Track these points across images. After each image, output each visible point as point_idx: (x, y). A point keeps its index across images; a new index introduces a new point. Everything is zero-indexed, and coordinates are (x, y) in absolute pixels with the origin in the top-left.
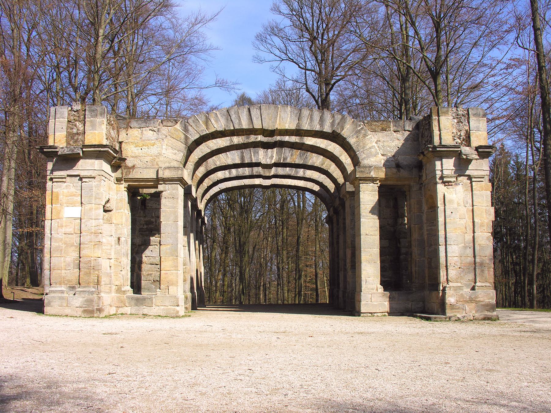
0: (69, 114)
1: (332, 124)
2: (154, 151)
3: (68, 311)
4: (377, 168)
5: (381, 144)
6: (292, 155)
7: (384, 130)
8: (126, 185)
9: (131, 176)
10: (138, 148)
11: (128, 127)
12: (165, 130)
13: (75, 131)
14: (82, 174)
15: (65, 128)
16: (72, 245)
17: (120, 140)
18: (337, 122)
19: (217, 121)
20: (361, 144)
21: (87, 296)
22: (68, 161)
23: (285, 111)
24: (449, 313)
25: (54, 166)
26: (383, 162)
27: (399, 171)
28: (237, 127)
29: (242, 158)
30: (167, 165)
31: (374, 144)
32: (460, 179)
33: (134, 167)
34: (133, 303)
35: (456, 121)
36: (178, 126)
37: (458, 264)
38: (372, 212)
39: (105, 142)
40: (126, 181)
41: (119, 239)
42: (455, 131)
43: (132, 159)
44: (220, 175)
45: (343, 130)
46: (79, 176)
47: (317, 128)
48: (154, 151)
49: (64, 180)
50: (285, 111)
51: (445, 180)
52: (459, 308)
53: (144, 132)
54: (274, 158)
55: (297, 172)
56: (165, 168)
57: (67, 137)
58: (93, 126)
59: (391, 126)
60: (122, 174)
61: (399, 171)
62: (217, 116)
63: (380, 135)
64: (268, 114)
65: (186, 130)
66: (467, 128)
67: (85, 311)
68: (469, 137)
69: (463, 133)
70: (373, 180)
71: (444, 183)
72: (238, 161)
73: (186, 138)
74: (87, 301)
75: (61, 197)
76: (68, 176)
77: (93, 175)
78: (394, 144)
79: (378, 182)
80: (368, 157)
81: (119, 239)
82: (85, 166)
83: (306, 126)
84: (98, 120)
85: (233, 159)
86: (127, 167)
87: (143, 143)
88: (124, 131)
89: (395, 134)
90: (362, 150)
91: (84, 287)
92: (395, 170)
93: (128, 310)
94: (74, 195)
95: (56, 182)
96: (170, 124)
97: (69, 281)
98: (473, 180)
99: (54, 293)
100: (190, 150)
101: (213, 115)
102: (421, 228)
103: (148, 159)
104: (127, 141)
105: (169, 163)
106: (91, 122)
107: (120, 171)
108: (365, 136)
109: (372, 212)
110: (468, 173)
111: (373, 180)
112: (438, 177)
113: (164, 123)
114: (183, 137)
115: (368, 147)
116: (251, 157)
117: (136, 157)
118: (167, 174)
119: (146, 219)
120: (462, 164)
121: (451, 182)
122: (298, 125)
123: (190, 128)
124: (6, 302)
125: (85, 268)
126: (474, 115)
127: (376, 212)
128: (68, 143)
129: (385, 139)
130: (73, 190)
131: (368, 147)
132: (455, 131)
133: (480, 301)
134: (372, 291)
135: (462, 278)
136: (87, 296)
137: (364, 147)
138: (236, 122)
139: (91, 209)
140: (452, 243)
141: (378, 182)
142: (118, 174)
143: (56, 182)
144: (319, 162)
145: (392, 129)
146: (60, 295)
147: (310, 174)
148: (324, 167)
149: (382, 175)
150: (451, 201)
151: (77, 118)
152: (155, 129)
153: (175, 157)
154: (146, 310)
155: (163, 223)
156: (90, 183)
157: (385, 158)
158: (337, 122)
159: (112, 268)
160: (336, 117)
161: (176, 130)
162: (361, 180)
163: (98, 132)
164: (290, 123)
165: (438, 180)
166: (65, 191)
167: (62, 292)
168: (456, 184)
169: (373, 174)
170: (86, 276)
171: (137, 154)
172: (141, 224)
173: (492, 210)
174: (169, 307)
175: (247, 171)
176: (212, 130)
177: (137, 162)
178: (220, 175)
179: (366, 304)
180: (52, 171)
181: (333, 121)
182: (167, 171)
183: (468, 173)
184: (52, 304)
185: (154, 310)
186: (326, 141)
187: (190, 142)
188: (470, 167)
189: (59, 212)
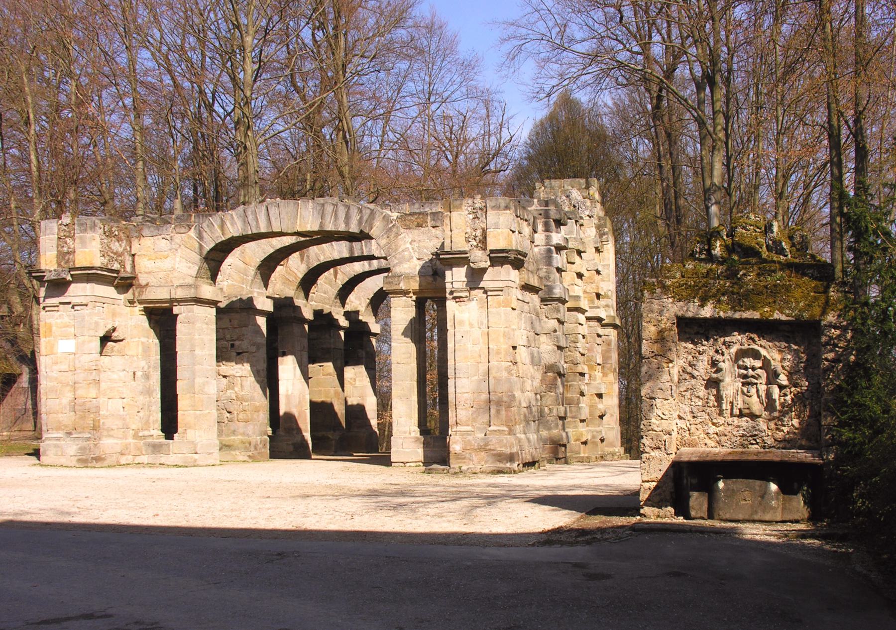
0: (59, 229)
1: (360, 222)
2: (166, 264)
3: (63, 461)
4: (408, 277)
5: (416, 245)
7: (419, 225)
8: (141, 307)
9: (144, 297)
11: (140, 236)
12: (178, 238)
13: (65, 249)
14: (75, 300)
15: (55, 246)
16: (68, 385)
17: (133, 253)
18: (365, 218)
19: (233, 223)
20: (393, 246)
21: (81, 443)
22: (58, 286)
23: (306, 208)
24: (454, 464)
25: (46, 291)
26: (418, 268)
27: (435, 280)
28: (254, 232)
29: (351, 250)
30: (181, 282)
31: (408, 245)
32: (473, 292)
33: (147, 284)
34: (150, 451)
35: (471, 216)
36: (192, 233)
37: (468, 402)
38: (405, 334)
39: (98, 264)
40: (140, 302)
41: (134, 374)
42: (469, 230)
43: (145, 275)
46: (69, 303)
47: (342, 228)
48: (166, 264)
49: (56, 309)
50: (306, 208)
51: (455, 294)
52: (464, 458)
53: (157, 241)
56: (177, 286)
57: (58, 257)
58: (83, 243)
59: (429, 221)
60: (134, 294)
61: (435, 280)
62: (233, 218)
63: (416, 233)
64: (287, 213)
65: (200, 237)
66: (484, 226)
67: (79, 460)
68: (485, 238)
69: (479, 233)
70: (405, 293)
71: (454, 298)
72: (346, 255)
73: (201, 247)
74: (80, 449)
75: (54, 329)
76: (61, 303)
77: (84, 302)
78: (431, 244)
79: (411, 295)
80: (400, 263)
81: (134, 374)
82: (78, 291)
83: (330, 227)
84: (89, 235)
85: (339, 252)
86: (140, 286)
87: (158, 256)
88: (137, 240)
89: (433, 230)
91: (80, 433)
92: (431, 279)
93: (145, 459)
94: (68, 326)
96: (183, 230)
97: (66, 426)
98: (489, 293)
99: (52, 442)
101: (229, 217)
103: (162, 274)
105: (184, 279)
106: (81, 238)
107: (131, 291)
108: (398, 235)
109: (405, 334)
110: (482, 285)
111: (405, 293)
112: (448, 291)
113: (178, 230)
114: (197, 245)
115: (400, 250)
116: (362, 249)
117: (150, 273)
118: (180, 294)
120: (475, 276)
123: (204, 234)
125: (79, 411)
126: (493, 208)
127: (409, 334)
128: (59, 265)
129: (422, 237)
130: (66, 320)
131: (400, 250)
132: (469, 230)
133: (490, 450)
134: (404, 435)
135: (474, 420)
136: (81, 443)
137: (396, 250)
138: (253, 224)
139: (84, 342)
140: (461, 376)
141: (411, 295)
142: (129, 295)
145: (429, 224)
146: (55, 442)
149: (415, 285)
150: (462, 323)
151: (68, 234)
152: (168, 237)
154: (163, 459)
157: (421, 263)
158: (365, 218)
161: (190, 237)
162: (391, 293)
163: (90, 249)
164: (312, 223)
165: (448, 296)
166: (59, 321)
167: (58, 439)
168: (469, 300)
169: (403, 286)
170: (88, 423)
171: (150, 269)
177: (152, 280)
179: (397, 451)
180: (45, 298)
181: (361, 218)
182: (180, 289)
183: (482, 285)
184: (48, 453)
185: (171, 459)
187: (205, 252)
188: (486, 277)
189: (52, 346)
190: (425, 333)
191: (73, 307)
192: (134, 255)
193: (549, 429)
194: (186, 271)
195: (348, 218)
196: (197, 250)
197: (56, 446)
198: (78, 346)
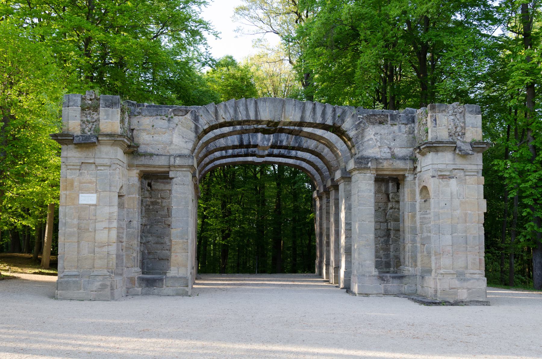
2: (165, 138)
6: (287, 139)
7: (381, 123)
10: (149, 135)
15: (78, 116)
17: (132, 127)
19: (226, 110)
29: (241, 140)
30: (178, 152)
31: (372, 136)
36: (189, 116)
44: (217, 154)
45: (344, 122)
47: (319, 120)
50: (432, 138)
54: (271, 141)
55: (289, 153)
63: (378, 128)
72: (237, 143)
73: (197, 127)
90: (360, 142)
95: (71, 169)
100: (199, 138)
102: (414, 216)
104: (138, 129)
114: (193, 126)
115: (366, 139)
117: (148, 144)
119: (153, 200)
121: (446, 175)
122: (302, 117)
124: (11, 279)
143: (71, 169)
144: (313, 145)
147: (300, 154)
148: (318, 150)
153: (184, 145)
155: (174, 207)
156: (106, 171)
159: (124, 251)
160: (337, 110)
172: (147, 205)
173: (484, 203)
174: (179, 288)
175: (243, 151)
176: (221, 121)
178: (217, 154)
182: (178, 159)
186: (322, 131)
190: (427, 82)
191: (96, 166)
192: (133, 130)
193: (363, 47)
194: (183, 145)
195: (324, 114)
196: (193, 129)
197: (74, 282)
198: (99, 199)
